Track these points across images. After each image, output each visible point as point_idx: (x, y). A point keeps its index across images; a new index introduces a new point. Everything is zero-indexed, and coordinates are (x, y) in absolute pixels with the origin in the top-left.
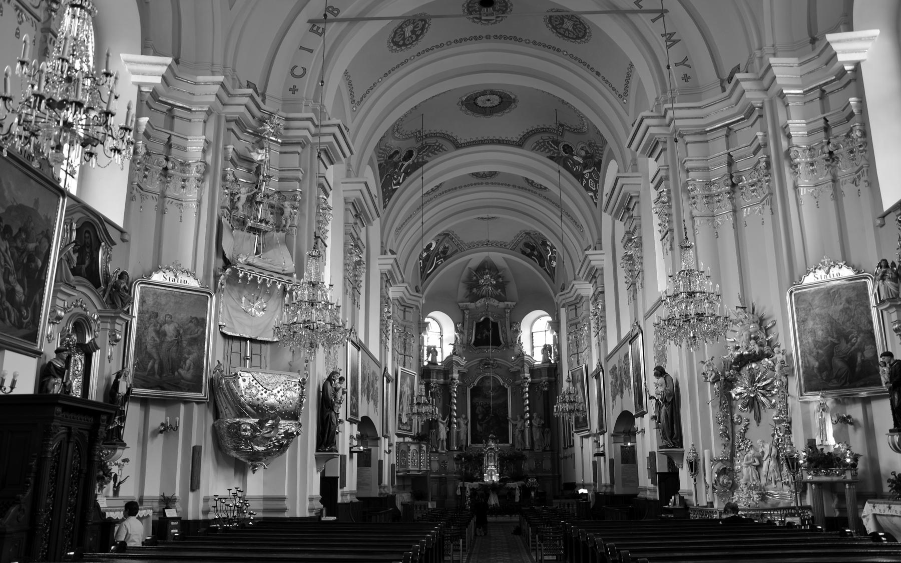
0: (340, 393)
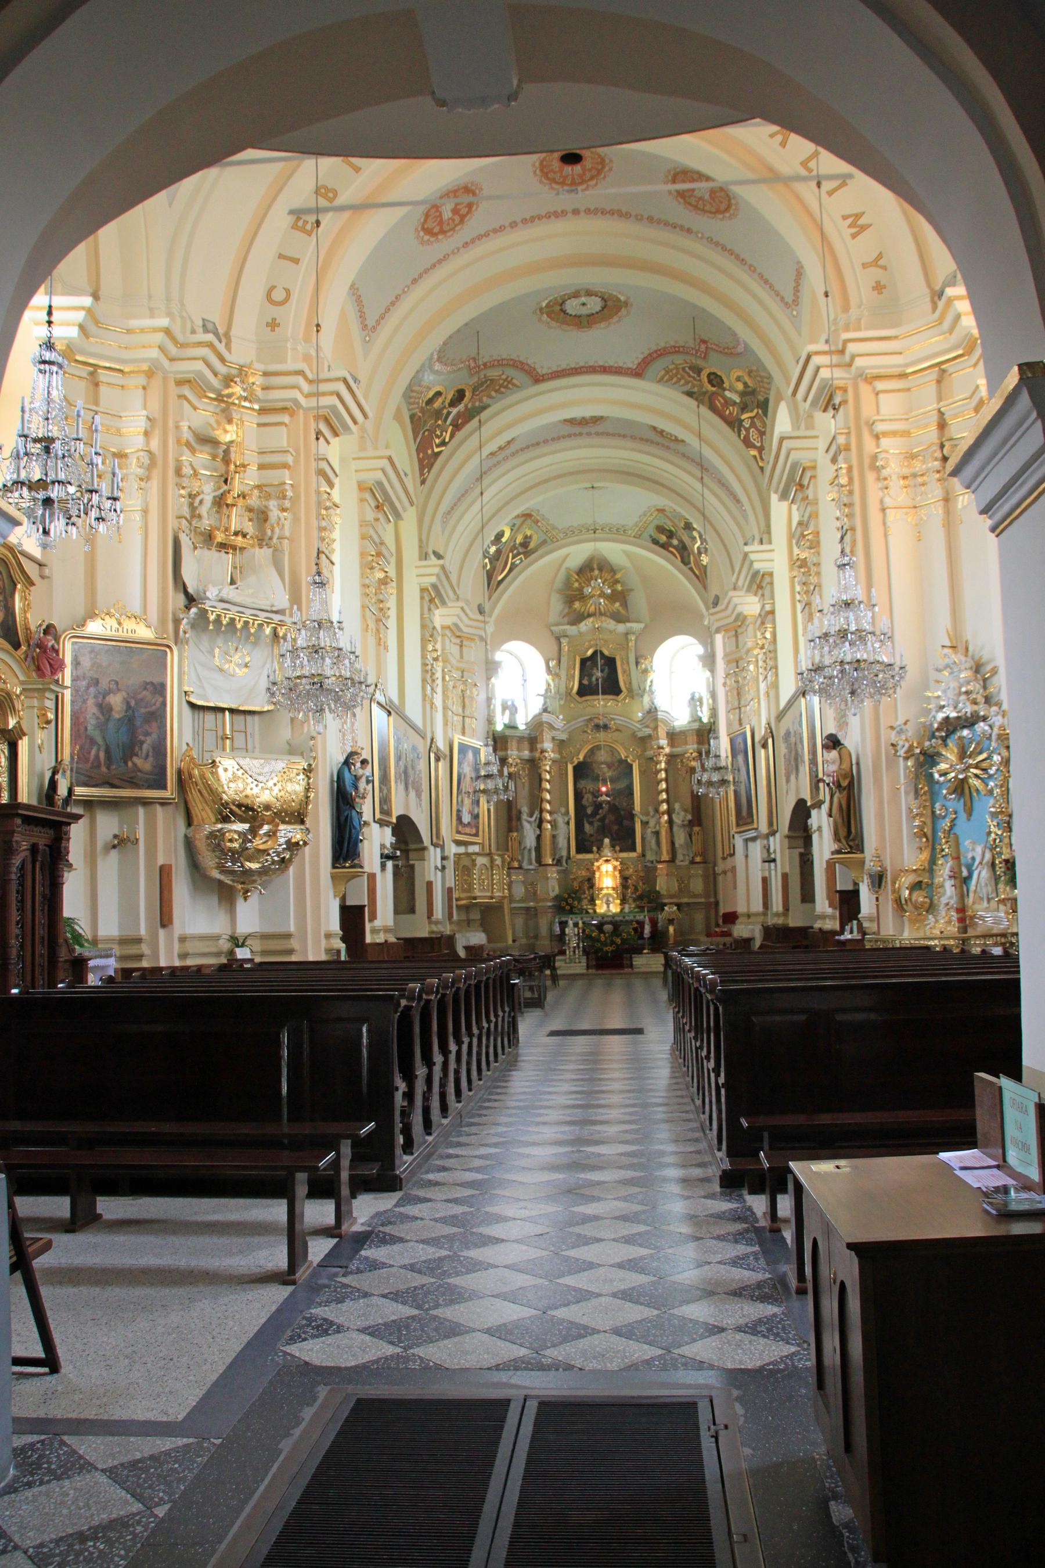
0: (362, 784)
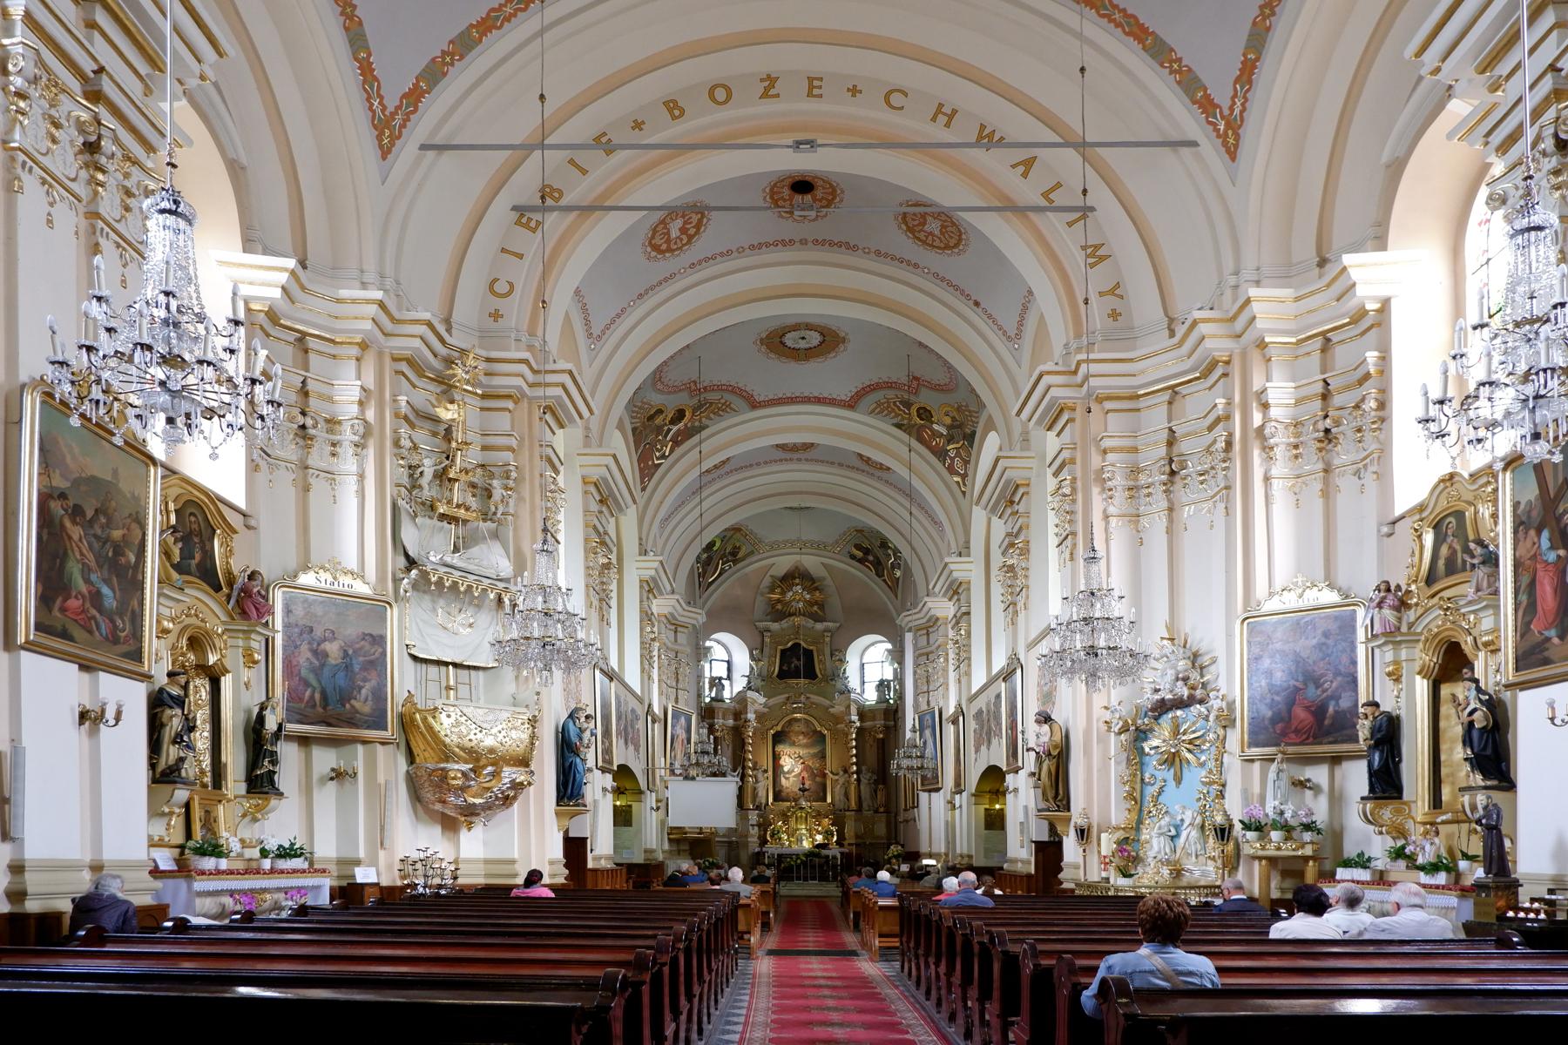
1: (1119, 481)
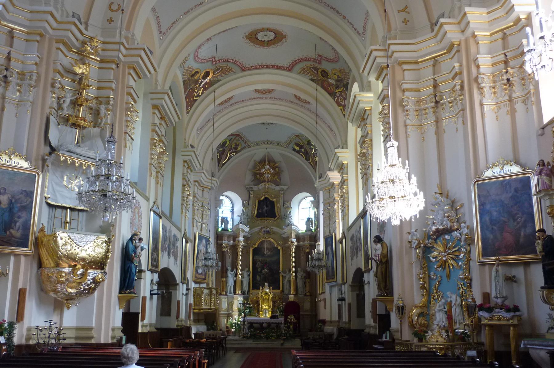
0: (139, 250)
1: (411, 107)
